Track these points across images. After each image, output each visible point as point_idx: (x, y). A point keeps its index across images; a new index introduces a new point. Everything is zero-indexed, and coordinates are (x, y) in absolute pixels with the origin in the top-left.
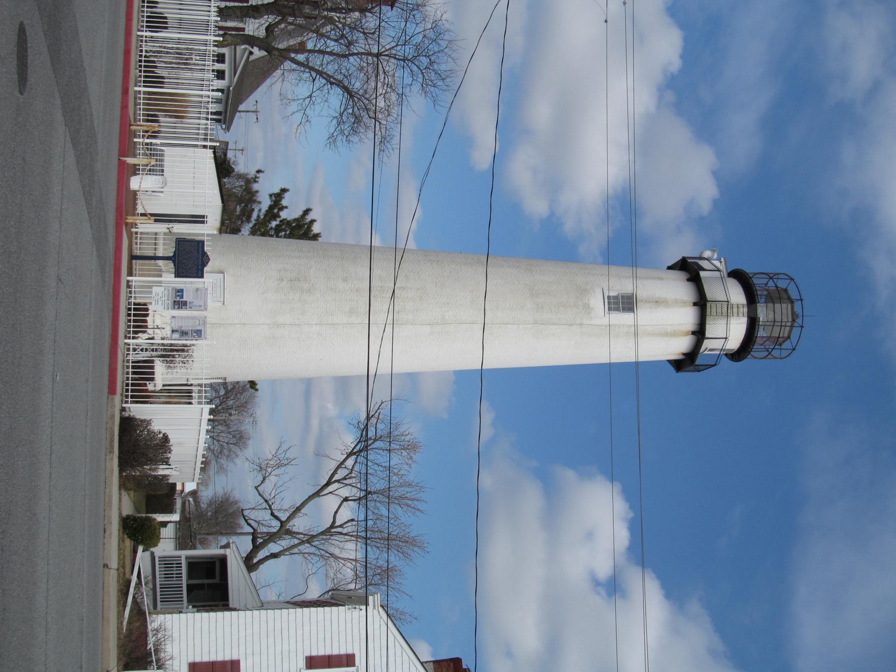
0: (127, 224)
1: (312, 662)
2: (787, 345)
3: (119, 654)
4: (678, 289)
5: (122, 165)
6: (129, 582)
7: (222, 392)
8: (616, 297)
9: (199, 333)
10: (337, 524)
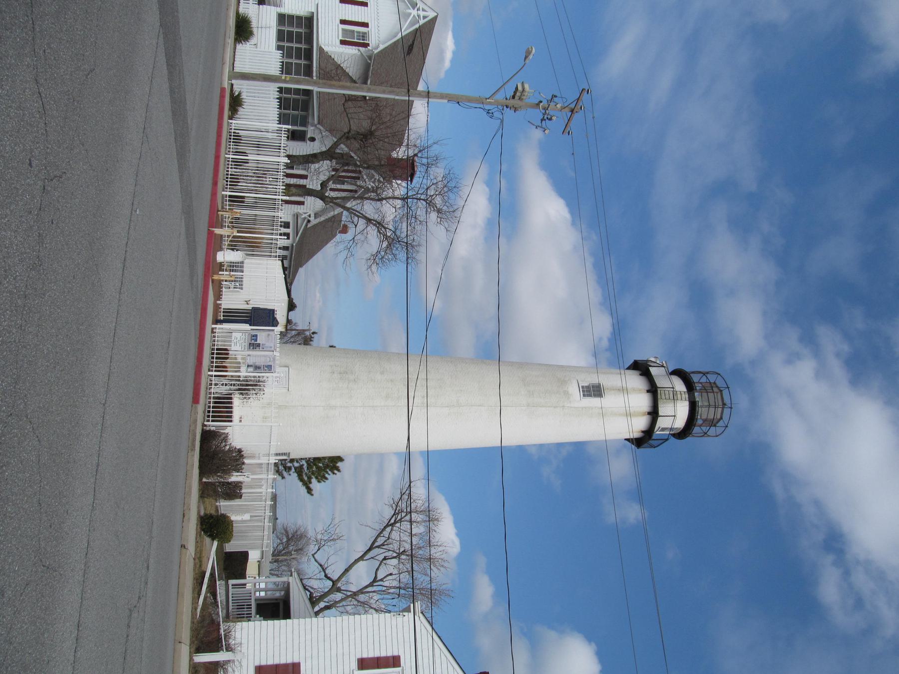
0: (213, 281)
1: (363, 664)
2: (721, 423)
3: (192, 637)
4: (636, 381)
5: (211, 234)
6: (204, 573)
7: (285, 540)
8: (588, 387)
9: (269, 368)
10: (379, 578)
